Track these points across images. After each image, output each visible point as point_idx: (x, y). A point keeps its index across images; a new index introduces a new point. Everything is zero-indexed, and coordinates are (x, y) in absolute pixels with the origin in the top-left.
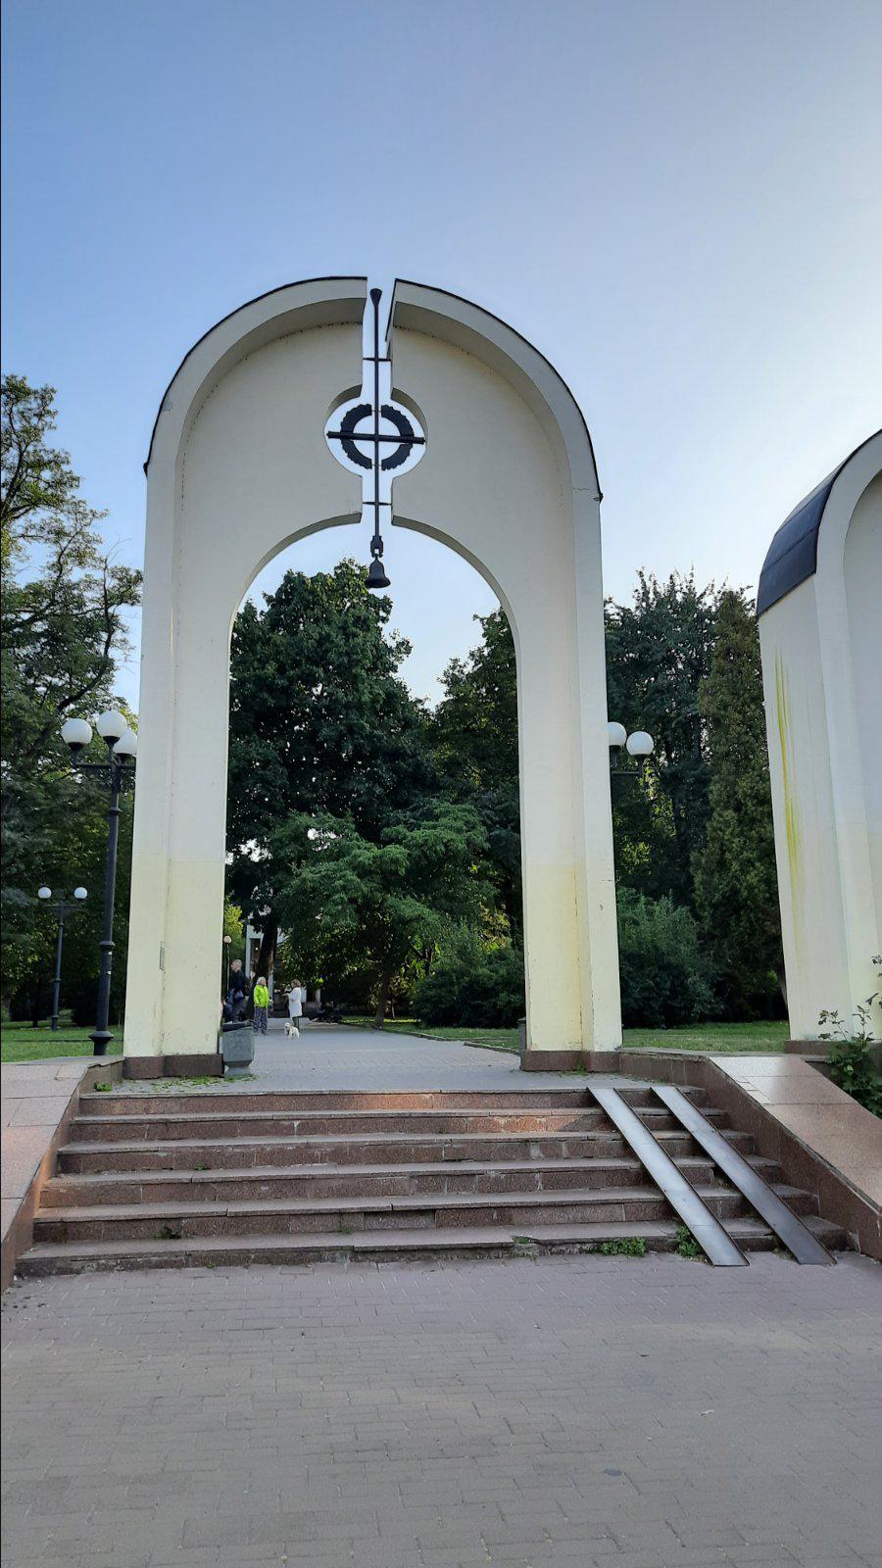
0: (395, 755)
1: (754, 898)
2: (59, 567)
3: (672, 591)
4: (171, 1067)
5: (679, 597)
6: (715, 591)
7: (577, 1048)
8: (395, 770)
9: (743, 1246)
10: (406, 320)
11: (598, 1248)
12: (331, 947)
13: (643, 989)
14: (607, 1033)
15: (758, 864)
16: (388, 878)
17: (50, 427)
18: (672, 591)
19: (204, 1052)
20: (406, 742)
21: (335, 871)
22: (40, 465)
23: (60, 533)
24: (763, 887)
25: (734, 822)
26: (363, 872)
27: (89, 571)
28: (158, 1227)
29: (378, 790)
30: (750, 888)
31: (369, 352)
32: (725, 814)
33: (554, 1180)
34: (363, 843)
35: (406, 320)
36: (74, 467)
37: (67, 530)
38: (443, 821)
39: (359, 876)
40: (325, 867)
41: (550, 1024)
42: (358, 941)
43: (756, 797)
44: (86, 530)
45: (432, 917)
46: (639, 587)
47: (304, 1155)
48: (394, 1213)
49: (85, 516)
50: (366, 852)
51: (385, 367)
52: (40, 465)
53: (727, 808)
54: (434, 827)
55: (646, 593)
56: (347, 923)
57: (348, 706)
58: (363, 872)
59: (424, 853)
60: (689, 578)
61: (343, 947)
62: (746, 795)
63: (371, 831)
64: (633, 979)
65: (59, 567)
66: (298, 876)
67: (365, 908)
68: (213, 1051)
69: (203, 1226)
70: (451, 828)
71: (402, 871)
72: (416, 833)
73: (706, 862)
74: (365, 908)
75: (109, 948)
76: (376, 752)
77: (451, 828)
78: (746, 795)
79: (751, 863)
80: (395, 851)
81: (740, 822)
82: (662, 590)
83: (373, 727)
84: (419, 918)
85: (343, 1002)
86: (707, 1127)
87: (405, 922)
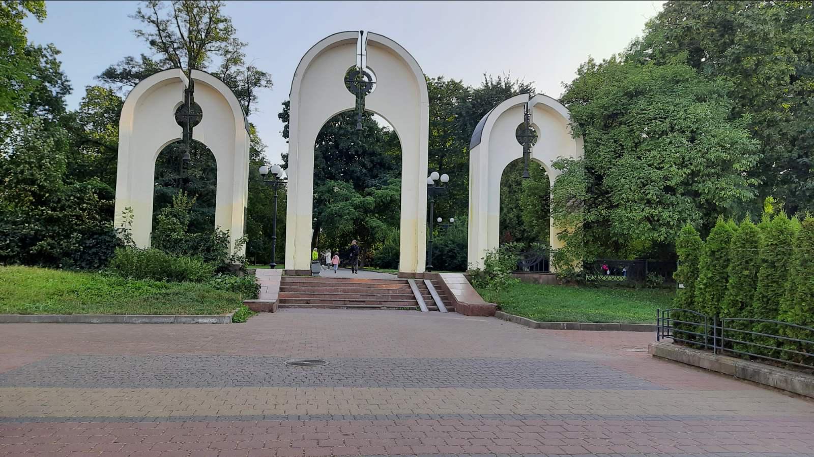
0: (373, 154)
1: (512, 224)
2: (226, 67)
3: (499, 83)
4: (297, 273)
5: (503, 84)
6: (519, 83)
7: (413, 272)
8: (372, 161)
9: (430, 310)
10: (370, 43)
11: (399, 309)
12: (342, 236)
13: (462, 257)
14: (421, 268)
15: (514, 210)
16: (365, 209)
17: (223, 5)
18: (499, 83)
19: (306, 269)
20: (377, 149)
21: (344, 206)
22: (219, 21)
23: (227, 52)
24: (515, 219)
25: (507, 192)
26: (356, 207)
27: (238, 67)
28: (305, 302)
29: (364, 171)
30: (510, 219)
31: (359, 52)
32: (504, 188)
33: (393, 297)
34: (358, 195)
35: (370, 43)
36: (235, 24)
37: (230, 50)
38: (391, 186)
39: (355, 209)
40: (340, 204)
41: (405, 265)
42: (354, 234)
43: (517, 182)
44: (238, 51)
45: (384, 226)
46: (485, 82)
47: (336, 290)
48: (357, 307)
49: (238, 45)
50: (358, 198)
51: (364, 58)
52: (219, 21)
53: (505, 186)
54: (387, 189)
55: (487, 83)
56: (350, 227)
57: (352, 133)
58: (356, 207)
59: (382, 200)
60: (508, 77)
61: (346, 237)
62: (512, 181)
63: (360, 187)
64: (459, 253)
65: (226, 67)
66: (329, 208)
67: (355, 221)
68: (309, 269)
69: (315, 301)
70: (393, 189)
71: (372, 208)
72: (379, 192)
73: (353, 248)
74: (355, 221)
75: (275, 238)
76: (365, 152)
77: (393, 189)
78: (512, 181)
79: (511, 209)
80: (370, 199)
81: (510, 192)
82: (494, 83)
83: (363, 143)
84: (378, 227)
85: (348, 260)
86: (433, 288)
87: (373, 228)
